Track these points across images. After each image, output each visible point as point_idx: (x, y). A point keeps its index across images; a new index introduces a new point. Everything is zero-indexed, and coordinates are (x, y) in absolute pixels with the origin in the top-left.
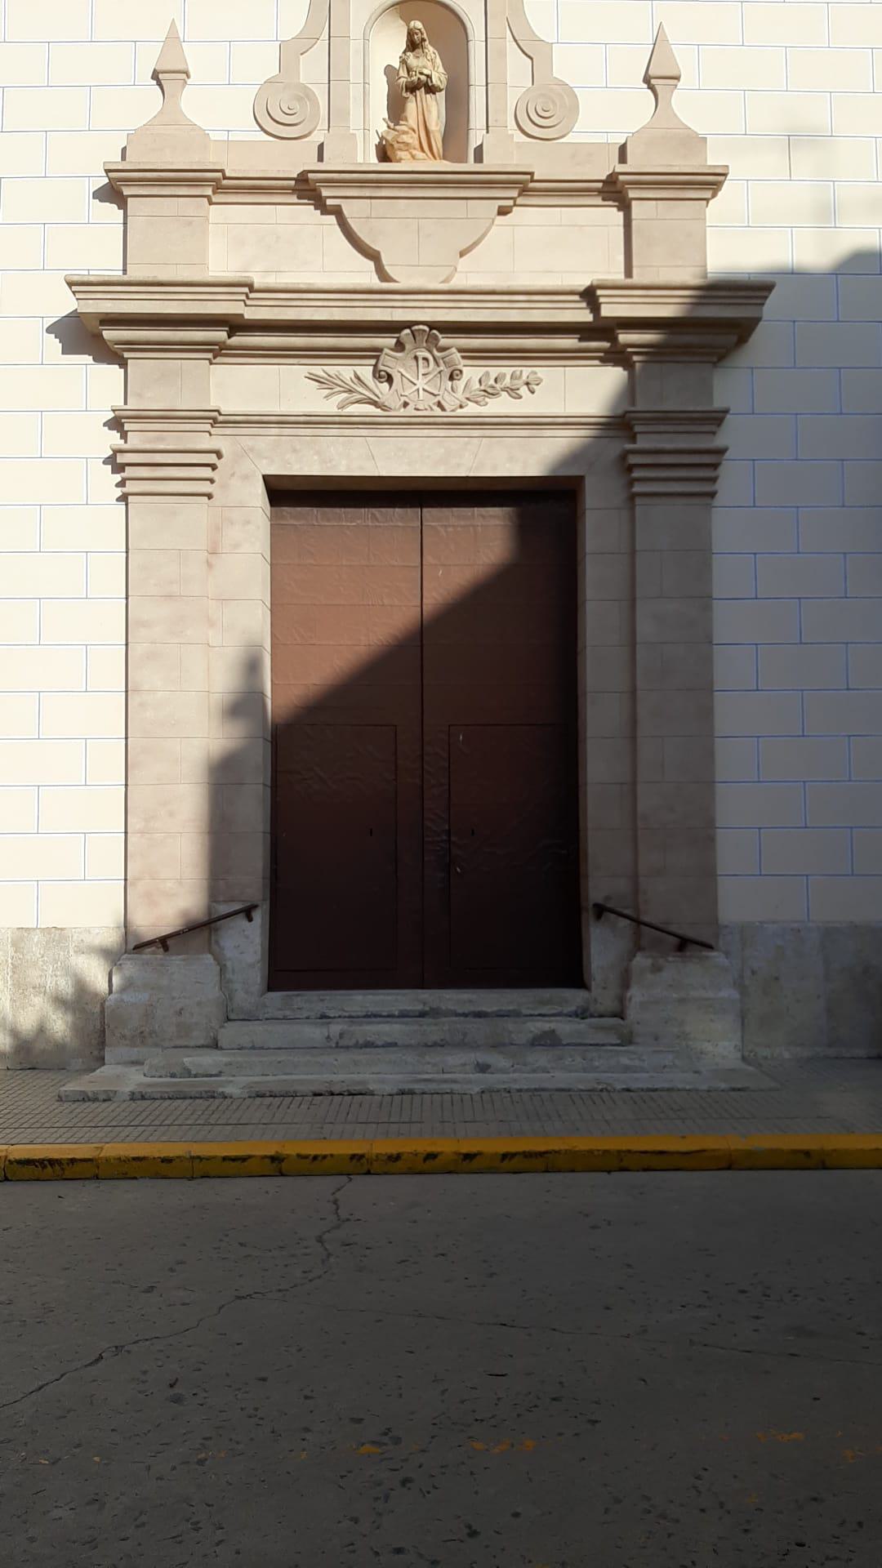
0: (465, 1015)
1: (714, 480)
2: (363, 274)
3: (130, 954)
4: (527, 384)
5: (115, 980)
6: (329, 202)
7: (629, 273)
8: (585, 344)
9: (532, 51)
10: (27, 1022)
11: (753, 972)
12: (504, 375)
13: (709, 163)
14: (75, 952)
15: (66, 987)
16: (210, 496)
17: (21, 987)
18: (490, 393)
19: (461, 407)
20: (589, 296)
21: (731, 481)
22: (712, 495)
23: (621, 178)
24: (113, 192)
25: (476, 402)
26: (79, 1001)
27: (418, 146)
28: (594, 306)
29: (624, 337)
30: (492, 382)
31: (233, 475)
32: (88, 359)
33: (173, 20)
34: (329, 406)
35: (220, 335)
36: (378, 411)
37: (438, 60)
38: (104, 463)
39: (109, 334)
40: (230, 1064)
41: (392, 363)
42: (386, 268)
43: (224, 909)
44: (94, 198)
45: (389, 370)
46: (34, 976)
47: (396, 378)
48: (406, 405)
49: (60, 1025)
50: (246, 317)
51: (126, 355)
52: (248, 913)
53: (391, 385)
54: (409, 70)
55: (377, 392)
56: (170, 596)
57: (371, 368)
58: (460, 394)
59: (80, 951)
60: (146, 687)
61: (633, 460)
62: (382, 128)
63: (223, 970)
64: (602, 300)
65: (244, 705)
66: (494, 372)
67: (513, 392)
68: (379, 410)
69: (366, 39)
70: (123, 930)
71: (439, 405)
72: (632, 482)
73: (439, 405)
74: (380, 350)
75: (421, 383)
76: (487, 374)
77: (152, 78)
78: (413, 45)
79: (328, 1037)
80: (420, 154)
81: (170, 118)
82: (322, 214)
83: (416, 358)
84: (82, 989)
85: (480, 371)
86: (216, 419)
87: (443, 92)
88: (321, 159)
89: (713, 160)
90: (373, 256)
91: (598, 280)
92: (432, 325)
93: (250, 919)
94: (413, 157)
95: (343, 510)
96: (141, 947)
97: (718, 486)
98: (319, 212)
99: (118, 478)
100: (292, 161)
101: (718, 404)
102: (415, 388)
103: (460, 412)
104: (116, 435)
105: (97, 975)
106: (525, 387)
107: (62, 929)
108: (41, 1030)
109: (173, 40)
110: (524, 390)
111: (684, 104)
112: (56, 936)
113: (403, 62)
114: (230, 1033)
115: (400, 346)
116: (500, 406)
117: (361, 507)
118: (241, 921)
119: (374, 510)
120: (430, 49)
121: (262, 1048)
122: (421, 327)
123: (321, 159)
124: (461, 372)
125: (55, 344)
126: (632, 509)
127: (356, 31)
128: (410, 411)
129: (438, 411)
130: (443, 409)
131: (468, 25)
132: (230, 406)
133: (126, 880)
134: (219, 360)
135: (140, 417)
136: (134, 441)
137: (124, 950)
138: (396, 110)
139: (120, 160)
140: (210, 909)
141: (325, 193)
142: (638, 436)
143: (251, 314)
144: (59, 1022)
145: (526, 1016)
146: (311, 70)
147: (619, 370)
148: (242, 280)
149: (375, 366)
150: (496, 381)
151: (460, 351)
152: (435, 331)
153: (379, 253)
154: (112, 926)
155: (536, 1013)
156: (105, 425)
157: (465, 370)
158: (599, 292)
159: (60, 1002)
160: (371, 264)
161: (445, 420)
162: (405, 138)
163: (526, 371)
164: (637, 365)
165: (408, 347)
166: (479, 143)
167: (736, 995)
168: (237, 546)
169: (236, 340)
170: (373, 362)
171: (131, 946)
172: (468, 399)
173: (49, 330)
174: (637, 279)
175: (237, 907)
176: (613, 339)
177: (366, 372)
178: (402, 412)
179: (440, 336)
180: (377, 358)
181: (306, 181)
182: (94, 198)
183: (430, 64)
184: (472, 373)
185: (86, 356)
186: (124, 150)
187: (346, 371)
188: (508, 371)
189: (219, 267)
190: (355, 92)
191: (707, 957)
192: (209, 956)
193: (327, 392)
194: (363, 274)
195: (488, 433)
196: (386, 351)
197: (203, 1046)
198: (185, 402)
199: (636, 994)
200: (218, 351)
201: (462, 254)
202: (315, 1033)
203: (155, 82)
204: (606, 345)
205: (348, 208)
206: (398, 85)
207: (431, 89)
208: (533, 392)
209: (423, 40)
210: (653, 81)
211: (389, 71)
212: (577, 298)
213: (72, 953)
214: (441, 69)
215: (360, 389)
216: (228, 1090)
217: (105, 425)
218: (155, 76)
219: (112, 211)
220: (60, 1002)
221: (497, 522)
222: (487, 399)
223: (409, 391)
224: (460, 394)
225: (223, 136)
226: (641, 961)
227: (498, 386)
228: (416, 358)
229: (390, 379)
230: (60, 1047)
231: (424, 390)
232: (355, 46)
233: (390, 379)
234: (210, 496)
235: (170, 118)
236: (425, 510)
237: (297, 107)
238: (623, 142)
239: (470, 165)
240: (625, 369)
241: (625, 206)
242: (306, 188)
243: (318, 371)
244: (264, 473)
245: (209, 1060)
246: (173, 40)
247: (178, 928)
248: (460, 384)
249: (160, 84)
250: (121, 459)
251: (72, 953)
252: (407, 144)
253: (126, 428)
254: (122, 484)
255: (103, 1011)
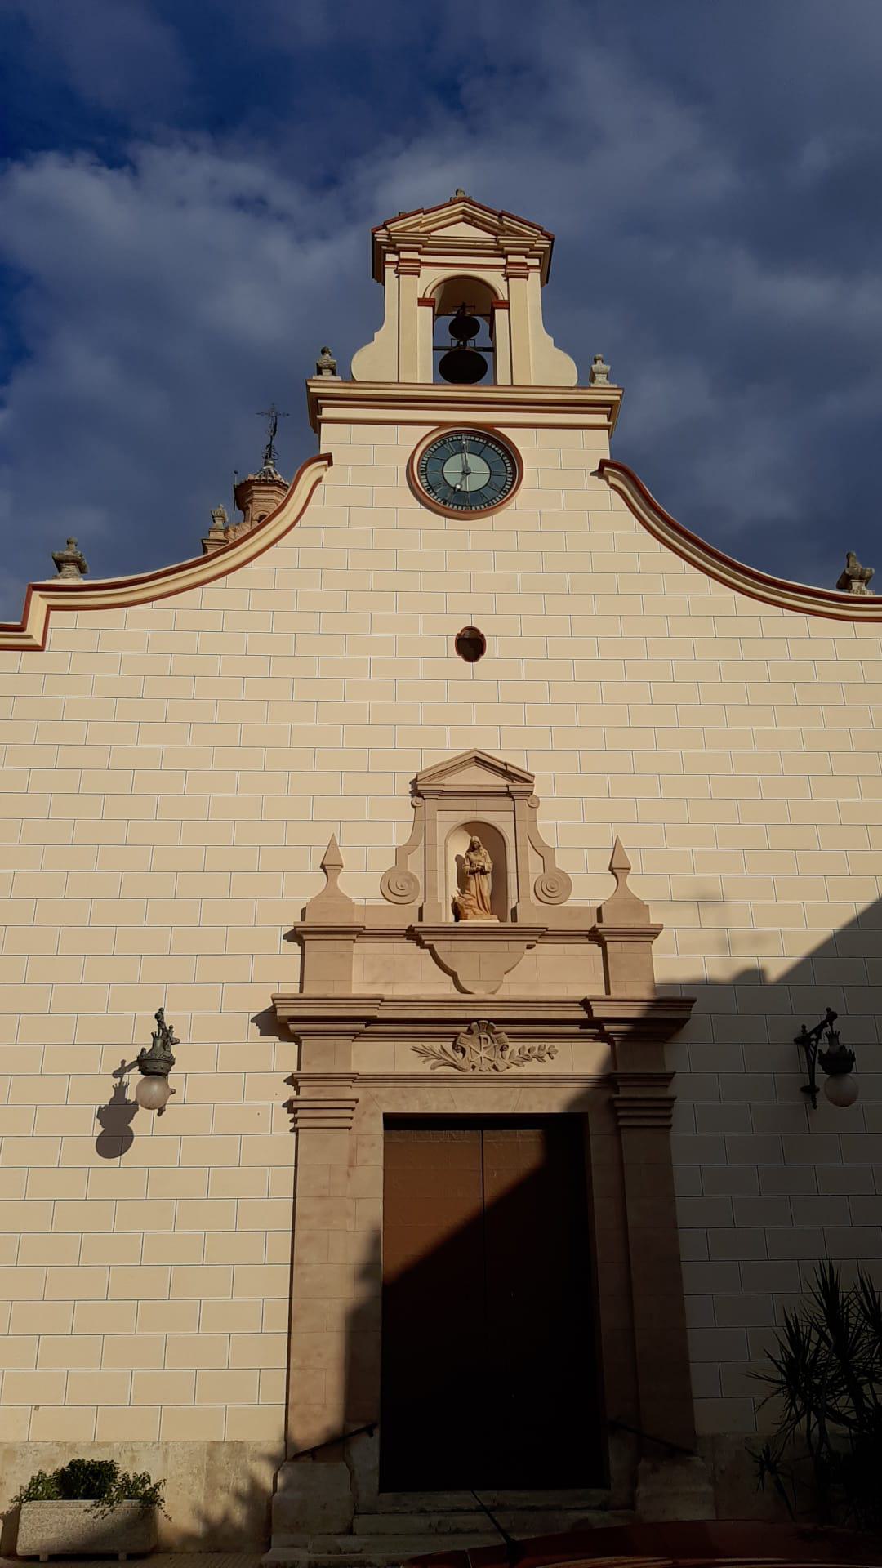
0: (521, 1509)
1: (670, 1117)
2: (447, 989)
3: (290, 1461)
4: (549, 1053)
5: (280, 1481)
6: (426, 943)
7: (608, 992)
8: (583, 1030)
9: (545, 854)
10: (216, 1512)
11: (722, 1472)
12: (534, 1048)
13: (651, 922)
14: (251, 1460)
15: (243, 1485)
16: (350, 1128)
17: (212, 1486)
18: (526, 1059)
19: (508, 1068)
20: (586, 1004)
21: (682, 1118)
22: (670, 1127)
23: (600, 930)
24: (295, 936)
25: (518, 1065)
26: (253, 1497)
27: (477, 905)
28: (589, 1010)
29: (607, 1028)
30: (526, 1052)
31: (365, 1113)
32: (276, 1039)
33: (333, 835)
34: (424, 1068)
35: (361, 1026)
36: (456, 1071)
37: (488, 856)
38: (284, 1106)
39: (293, 1027)
40: (367, 1544)
41: (467, 1042)
42: (461, 982)
43: (354, 1428)
44: (284, 939)
45: (464, 1046)
46: (222, 1478)
47: (468, 1050)
48: (474, 1067)
49: (239, 1515)
50: (379, 1016)
51: (301, 1038)
52: (369, 1431)
53: (464, 1055)
54: (471, 863)
55: (456, 1058)
56: (322, 1197)
57: (451, 1043)
58: (507, 1060)
59: (253, 1459)
60: (306, 1261)
61: (618, 1104)
62: (456, 895)
63: (352, 1473)
64: (593, 1007)
65: (367, 1272)
66: (528, 1046)
67: (540, 1059)
68: (456, 1070)
69: (446, 846)
70: (284, 1443)
71: (494, 1067)
72: (618, 1118)
73: (494, 1067)
74: (458, 1034)
75: (483, 1053)
76: (524, 1047)
77: (321, 867)
78: (473, 848)
79: (430, 1526)
80: (477, 910)
81: (331, 891)
82: (421, 948)
83: (480, 1038)
84: (255, 1485)
85: (520, 1045)
86: (356, 1078)
87: (490, 874)
88: (421, 919)
89: (654, 920)
90: (454, 975)
91: (591, 996)
92: (490, 1020)
93: (371, 1435)
94: (475, 913)
95: (431, 1132)
96: (298, 1456)
97: (672, 1121)
98: (419, 947)
99: (292, 1116)
100: (406, 918)
101: (668, 1069)
102: (479, 1056)
103: (507, 1072)
104: (291, 1088)
105: (265, 1474)
106: (547, 1055)
107: (242, 1442)
108: (226, 1518)
109: (332, 846)
110: (547, 1058)
111: (631, 882)
112: (237, 1447)
113: (467, 857)
114: (360, 1522)
115: (470, 1032)
116: (532, 1068)
117: (442, 1130)
118: (365, 1438)
119: (451, 1132)
120: (483, 850)
121: (384, 1534)
122: (484, 1021)
123: (421, 919)
124: (508, 1046)
125: (256, 1029)
126: (619, 1136)
127: (440, 841)
128: (477, 1071)
129: (494, 1072)
130: (497, 1070)
131: (505, 837)
132: (364, 1069)
133: (287, 1404)
134: (357, 1039)
135: (309, 1077)
136: (304, 1094)
137: (283, 1458)
138: (463, 881)
139: (300, 920)
140: (344, 1428)
141: (424, 938)
142: (621, 1089)
143: (380, 1014)
144: (238, 1514)
145: (566, 1509)
146: (414, 865)
147: (605, 1044)
148: (379, 996)
149: (454, 1043)
150: (529, 1051)
151: (507, 1034)
152: (492, 1024)
153: (456, 973)
154: (276, 1440)
155: (573, 1507)
156: (285, 1081)
157: (510, 1044)
158: (591, 1003)
159: (239, 1496)
160: (451, 979)
161: (500, 1077)
162: (470, 903)
163: (548, 1045)
164: (617, 1043)
165: (475, 1032)
166: (514, 906)
167: (711, 1489)
168: (366, 1161)
169: (370, 1028)
170: (453, 1040)
171: (291, 1454)
172: (512, 1063)
173: (252, 1021)
174: (614, 994)
175: (361, 1426)
176: (602, 1028)
177: (448, 1046)
178: (470, 1071)
179: (494, 1025)
180: (456, 1038)
181: (413, 931)
182: (284, 939)
183: (484, 860)
184: (514, 1046)
185: (275, 1037)
186: (304, 911)
187: (436, 1046)
188: (536, 1045)
189: (359, 986)
190: (440, 876)
191: (689, 1461)
192: (344, 1464)
193: (424, 1058)
194: (447, 989)
195: (525, 1085)
196: (462, 1034)
197: (340, 1534)
198: (338, 1069)
199: (642, 1490)
200: (357, 1035)
201: (505, 973)
202: (420, 1522)
203: (322, 870)
204: (597, 1031)
205: (437, 947)
206: (465, 870)
207: (483, 872)
208: (552, 1058)
209: (480, 846)
210: (615, 871)
211: (458, 858)
212: (577, 1005)
213: (248, 1461)
214: (490, 861)
215: (447, 1058)
216: (373, 1561)
217: (285, 1081)
218: (323, 867)
219: (295, 948)
220: (239, 1496)
221: (533, 1140)
222: (524, 1063)
223: (476, 1058)
224: (507, 1060)
225: (363, 903)
226: (644, 1465)
227: (530, 1055)
228: (480, 1038)
229: (464, 1051)
230: (239, 1532)
231: (485, 1058)
232: (440, 849)
233: (464, 1051)
234: (350, 1128)
235: (331, 891)
236: (484, 1132)
237: (405, 884)
238: (599, 906)
239: (509, 923)
240: (609, 1044)
241: (603, 944)
242: (412, 935)
243: (419, 1045)
244: (385, 1112)
245: (351, 1542)
246: (332, 846)
247: (323, 1442)
248: (507, 1053)
249: (325, 871)
250: (295, 1105)
251: (248, 1461)
252: (471, 906)
253: (299, 1084)
254: (294, 1120)
255: (269, 1505)
